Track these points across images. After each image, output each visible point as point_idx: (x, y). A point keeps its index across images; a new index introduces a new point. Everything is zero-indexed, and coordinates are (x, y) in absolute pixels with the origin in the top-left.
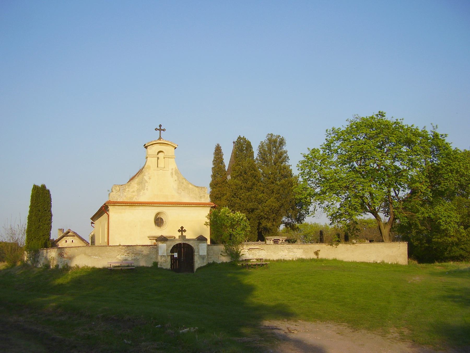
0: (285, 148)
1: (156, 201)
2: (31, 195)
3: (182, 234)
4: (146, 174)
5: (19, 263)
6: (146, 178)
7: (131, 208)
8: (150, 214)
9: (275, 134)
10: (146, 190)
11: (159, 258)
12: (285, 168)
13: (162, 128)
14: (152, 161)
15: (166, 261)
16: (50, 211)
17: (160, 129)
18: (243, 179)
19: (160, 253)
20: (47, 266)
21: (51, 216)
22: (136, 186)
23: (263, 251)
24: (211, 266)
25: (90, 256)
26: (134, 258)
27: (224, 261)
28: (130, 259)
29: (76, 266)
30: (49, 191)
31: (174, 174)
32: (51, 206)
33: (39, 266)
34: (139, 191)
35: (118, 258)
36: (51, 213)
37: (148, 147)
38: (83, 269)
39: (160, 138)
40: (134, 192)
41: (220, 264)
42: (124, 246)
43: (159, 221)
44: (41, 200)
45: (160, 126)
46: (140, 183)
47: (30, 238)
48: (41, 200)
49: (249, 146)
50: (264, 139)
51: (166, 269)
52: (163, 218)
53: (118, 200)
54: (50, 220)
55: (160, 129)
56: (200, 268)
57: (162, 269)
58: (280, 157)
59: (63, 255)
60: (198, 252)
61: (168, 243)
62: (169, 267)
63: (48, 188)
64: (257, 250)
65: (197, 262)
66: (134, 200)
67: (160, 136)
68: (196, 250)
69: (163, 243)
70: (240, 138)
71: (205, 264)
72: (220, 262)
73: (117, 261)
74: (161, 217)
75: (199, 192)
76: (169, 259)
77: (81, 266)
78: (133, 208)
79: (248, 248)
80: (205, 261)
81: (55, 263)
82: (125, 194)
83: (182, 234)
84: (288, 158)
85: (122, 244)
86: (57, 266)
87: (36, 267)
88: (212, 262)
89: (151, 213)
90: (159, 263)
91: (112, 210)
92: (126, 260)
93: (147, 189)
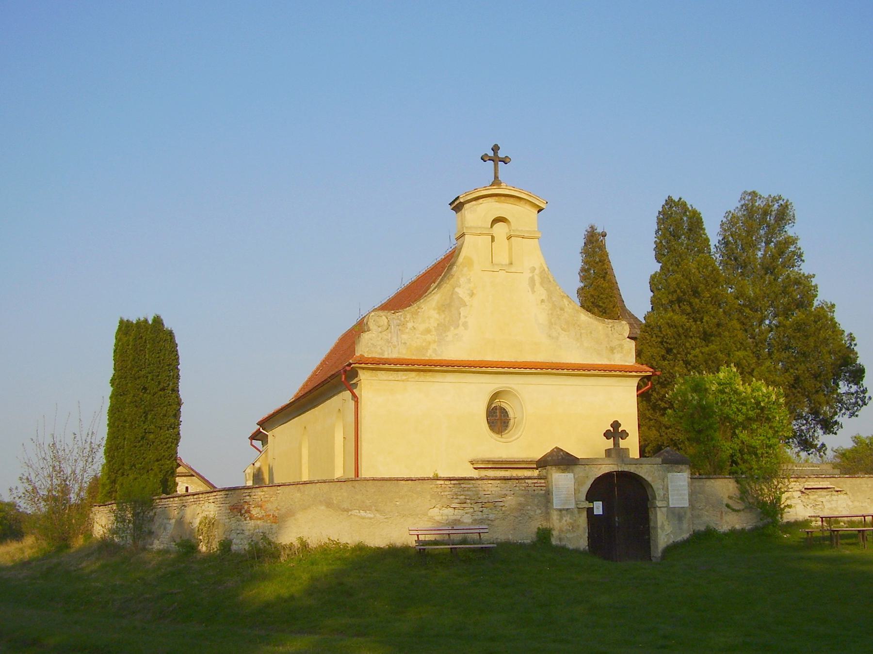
0: (790, 231)
1: (489, 358)
2: (113, 347)
3: (616, 444)
4: (462, 280)
5: (79, 542)
6: (462, 292)
7: (423, 377)
8: (473, 394)
9: (765, 192)
10: (461, 328)
11: (555, 516)
12: (797, 282)
13: (501, 154)
14: (474, 248)
15: (574, 527)
16: (175, 390)
17: (495, 157)
18: (689, 310)
19: (556, 504)
20: (189, 547)
21: (179, 404)
22: (434, 314)
23: (842, 496)
24: (704, 538)
25: (347, 510)
26: (479, 516)
27: (738, 527)
28: (467, 519)
29: (296, 543)
30: (171, 334)
31: (537, 284)
32: (178, 377)
33: (157, 545)
34: (442, 328)
35: (431, 518)
36: (178, 397)
37: (467, 206)
38: (324, 550)
39: (496, 182)
40: (428, 331)
41: (725, 534)
42: (450, 479)
43: (498, 419)
44: (146, 362)
45: (495, 149)
46: (443, 308)
47: (116, 466)
48: (146, 362)
49: (696, 222)
50: (733, 204)
51: (576, 551)
52: (508, 409)
53: (386, 356)
54: (177, 415)
55: (495, 157)
56: (672, 549)
57: (562, 550)
58: (781, 253)
59: (248, 511)
60: (666, 498)
61: (578, 469)
62: (582, 543)
63: (168, 324)
64: (824, 492)
65: (663, 526)
66: (431, 355)
67: (496, 177)
68: (659, 493)
69: (564, 471)
70: (670, 202)
71: (685, 536)
72: (724, 528)
73: (429, 525)
74: (504, 405)
75: (607, 336)
76: (582, 520)
77: (313, 543)
78: (429, 377)
79: (801, 487)
80: (685, 526)
81: (218, 535)
82: (405, 337)
83: (616, 444)
84: (800, 256)
85: (442, 474)
86: (226, 545)
87: (144, 549)
88: (702, 528)
89: (475, 393)
90: (555, 533)
91: (369, 385)
92: (457, 522)
93: (465, 325)
